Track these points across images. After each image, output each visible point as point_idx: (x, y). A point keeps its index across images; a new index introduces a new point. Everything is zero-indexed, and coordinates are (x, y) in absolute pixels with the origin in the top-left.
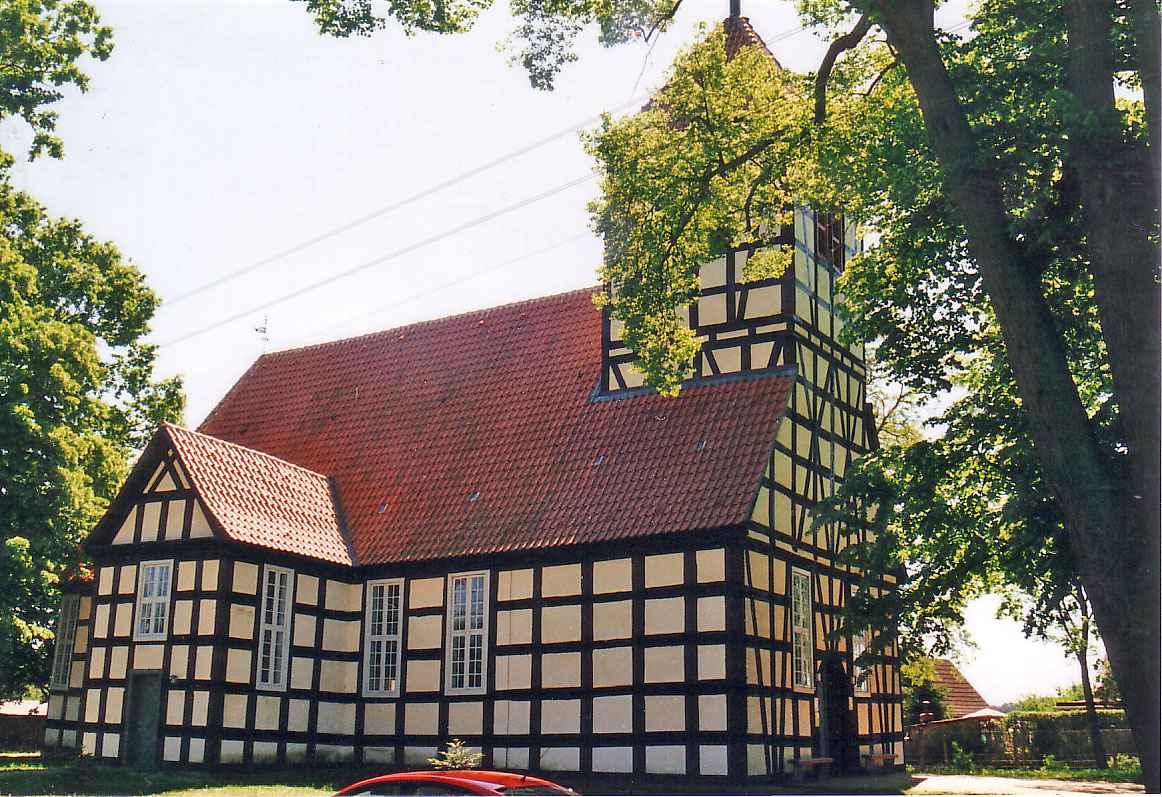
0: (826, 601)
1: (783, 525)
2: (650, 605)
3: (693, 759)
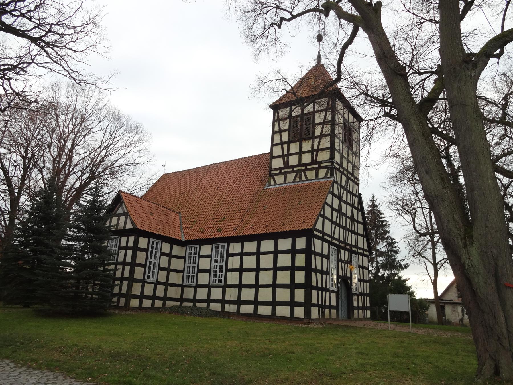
0: (343, 258)
1: (328, 230)
2: (280, 256)
3: (292, 311)
